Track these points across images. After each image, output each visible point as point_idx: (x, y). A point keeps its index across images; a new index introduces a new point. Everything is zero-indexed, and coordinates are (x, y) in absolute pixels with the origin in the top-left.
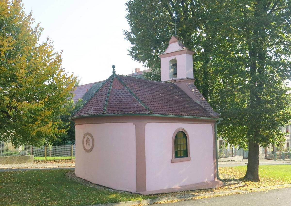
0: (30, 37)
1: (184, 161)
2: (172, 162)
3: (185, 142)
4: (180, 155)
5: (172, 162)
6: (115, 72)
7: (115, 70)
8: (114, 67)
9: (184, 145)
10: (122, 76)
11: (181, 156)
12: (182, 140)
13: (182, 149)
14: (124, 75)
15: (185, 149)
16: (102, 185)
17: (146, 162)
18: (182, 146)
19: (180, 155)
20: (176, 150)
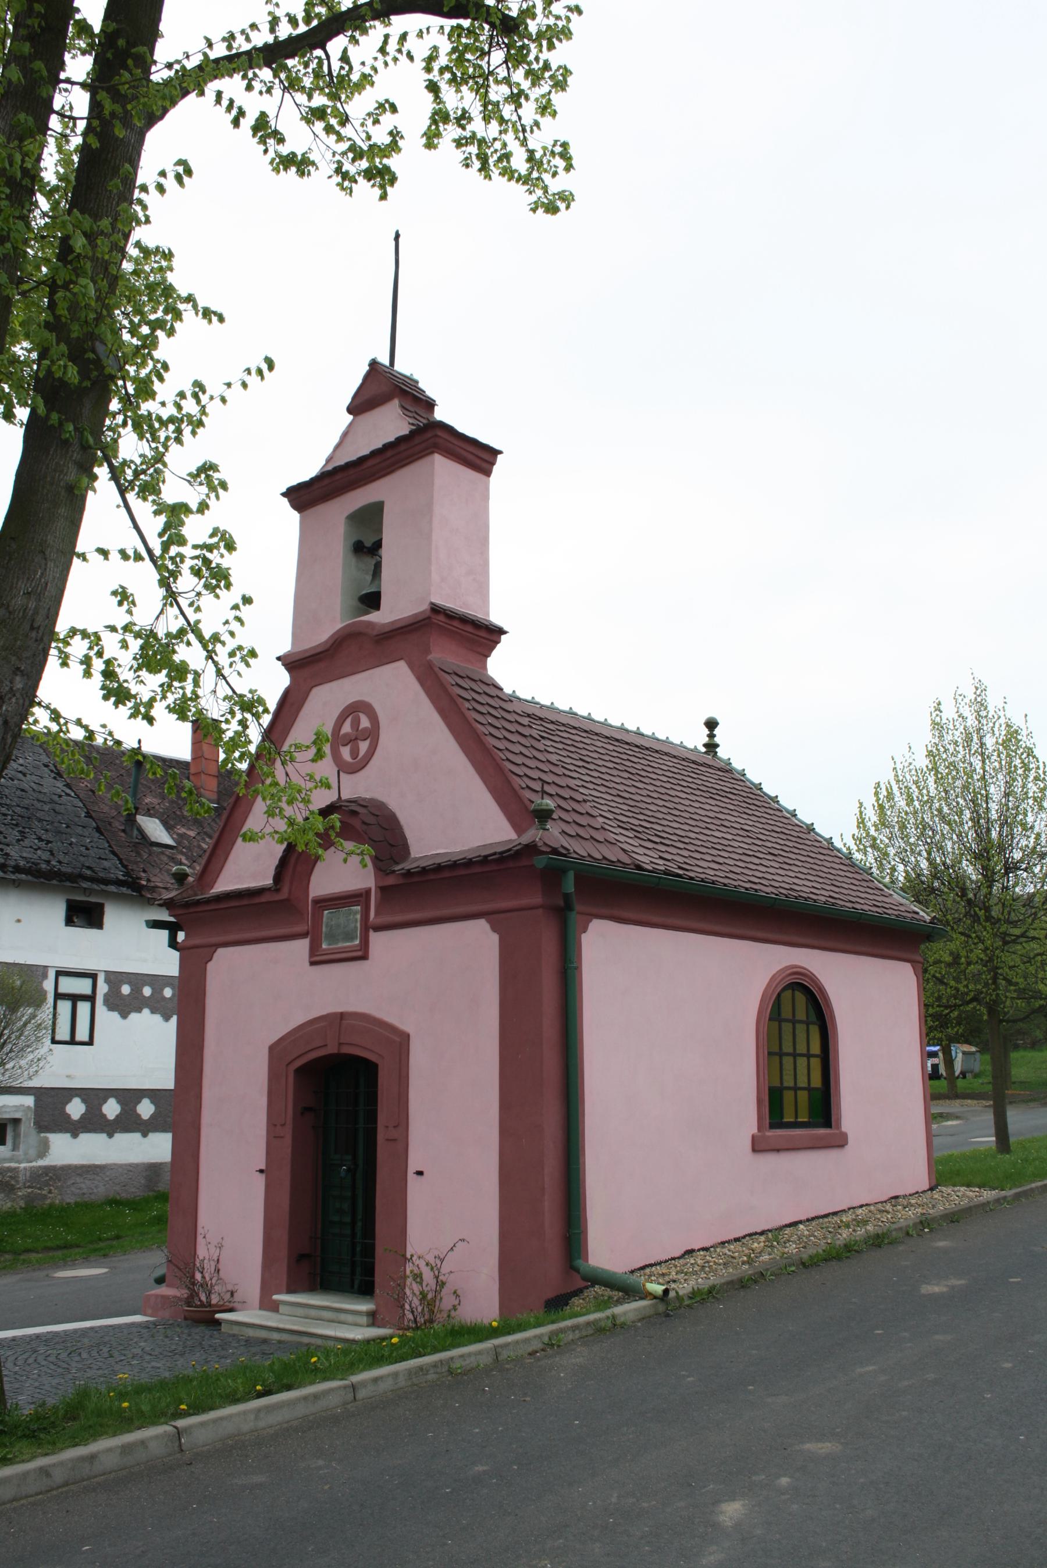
0: (189, 306)
1: (778, 1151)
2: (758, 1146)
3: (816, 1048)
4: (796, 1117)
5: (758, 1146)
6: (717, 746)
7: (717, 740)
8: (711, 725)
9: (798, 1058)
10: (810, 829)
11: (799, 1120)
12: (801, 1029)
13: (802, 1082)
14: (766, 789)
15: (817, 1082)
16: (827, 1212)
17: (379, 1076)
18: (802, 1062)
19: (796, 1117)
20: (776, 1083)
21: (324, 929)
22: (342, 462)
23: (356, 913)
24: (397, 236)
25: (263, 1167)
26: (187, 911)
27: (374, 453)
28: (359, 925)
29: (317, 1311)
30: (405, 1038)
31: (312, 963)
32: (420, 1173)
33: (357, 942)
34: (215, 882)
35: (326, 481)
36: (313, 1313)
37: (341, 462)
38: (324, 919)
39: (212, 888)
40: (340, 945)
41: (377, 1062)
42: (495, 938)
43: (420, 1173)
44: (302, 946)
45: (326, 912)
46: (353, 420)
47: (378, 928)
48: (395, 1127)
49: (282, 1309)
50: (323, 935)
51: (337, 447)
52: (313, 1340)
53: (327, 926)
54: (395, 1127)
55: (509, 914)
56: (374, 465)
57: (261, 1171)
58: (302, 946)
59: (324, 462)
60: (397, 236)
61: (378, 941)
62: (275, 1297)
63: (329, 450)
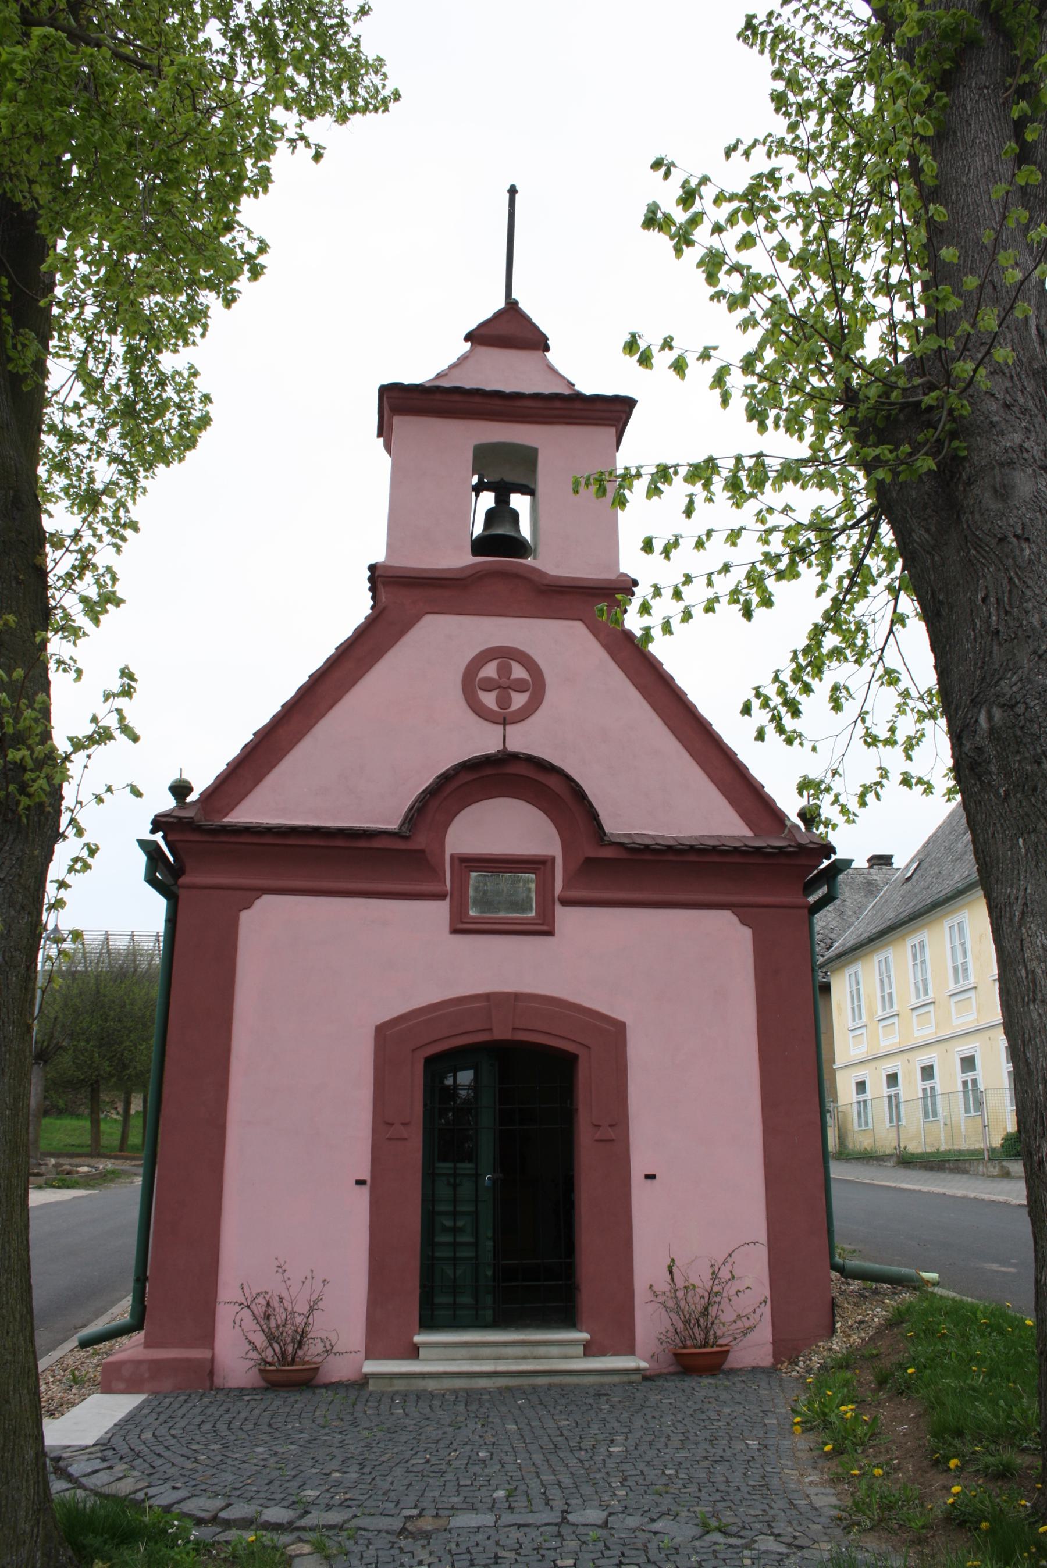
21: (471, 893)
22: (468, 384)
23: (529, 881)
24: (513, 191)
25: (366, 1176)
26: (322, 843)
27: (537, 397)
28: (533, 895)
29: (531, 1348)
30: (619, 1029)
31: (455, 931)
32: (650, 1177)
33: (533, 914)
34: (232, 809)
35: (457, 398)
36: (474, 1351)
37: (445, 383)
38: (471, 882)
39: (226, 815)
40: (502, 915)
41: (576, 1052)
42: (747, 933)
43: (650, 1177)
44: (439, 911)
45: (473, 875)
46: (471, 351)
47: (566, 902)
48: (611, 1126)
49: (423, 1352)
50: (470, 901)
51: (452, 367)
52: (556, 1380)
53: (476, 889)
54: (611, 1126)
55: (745, 909)
56: (531, 408)
57: (360, 1183)
58: (439, 911)
59: (432, 376)
60: (513, 191)
61: (566, 918)
62: (417, 1339)
63: (444, 366)
